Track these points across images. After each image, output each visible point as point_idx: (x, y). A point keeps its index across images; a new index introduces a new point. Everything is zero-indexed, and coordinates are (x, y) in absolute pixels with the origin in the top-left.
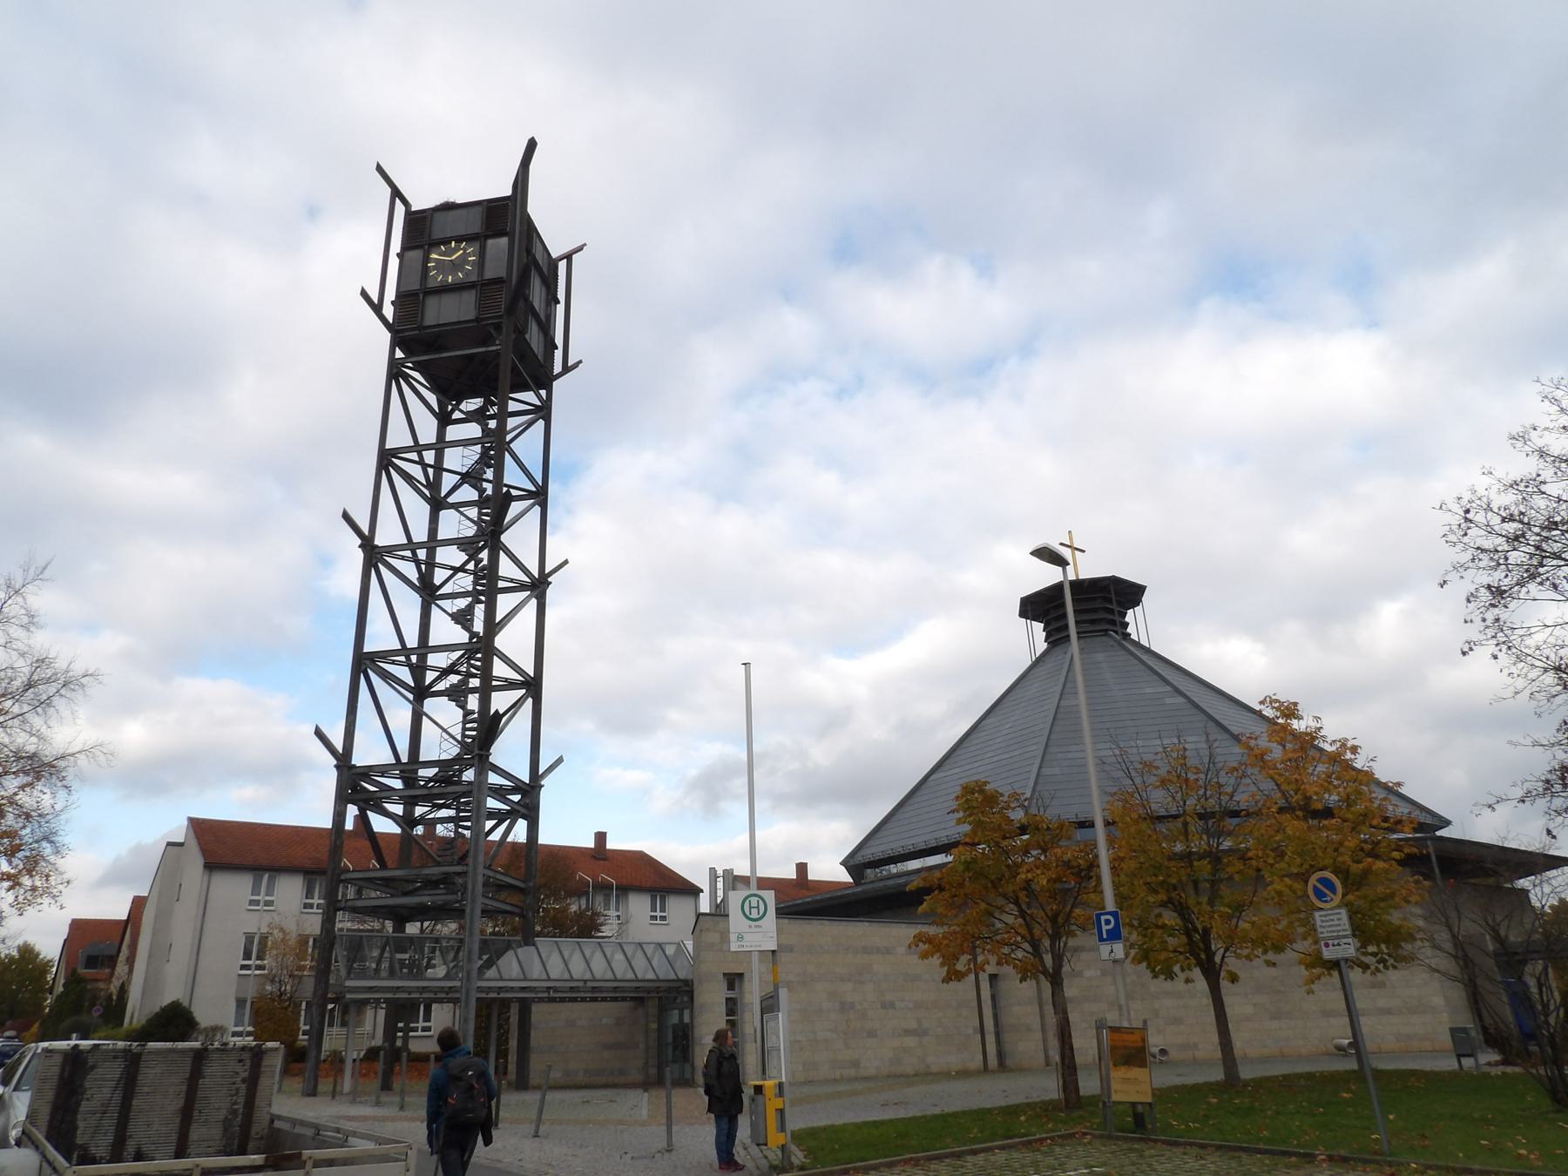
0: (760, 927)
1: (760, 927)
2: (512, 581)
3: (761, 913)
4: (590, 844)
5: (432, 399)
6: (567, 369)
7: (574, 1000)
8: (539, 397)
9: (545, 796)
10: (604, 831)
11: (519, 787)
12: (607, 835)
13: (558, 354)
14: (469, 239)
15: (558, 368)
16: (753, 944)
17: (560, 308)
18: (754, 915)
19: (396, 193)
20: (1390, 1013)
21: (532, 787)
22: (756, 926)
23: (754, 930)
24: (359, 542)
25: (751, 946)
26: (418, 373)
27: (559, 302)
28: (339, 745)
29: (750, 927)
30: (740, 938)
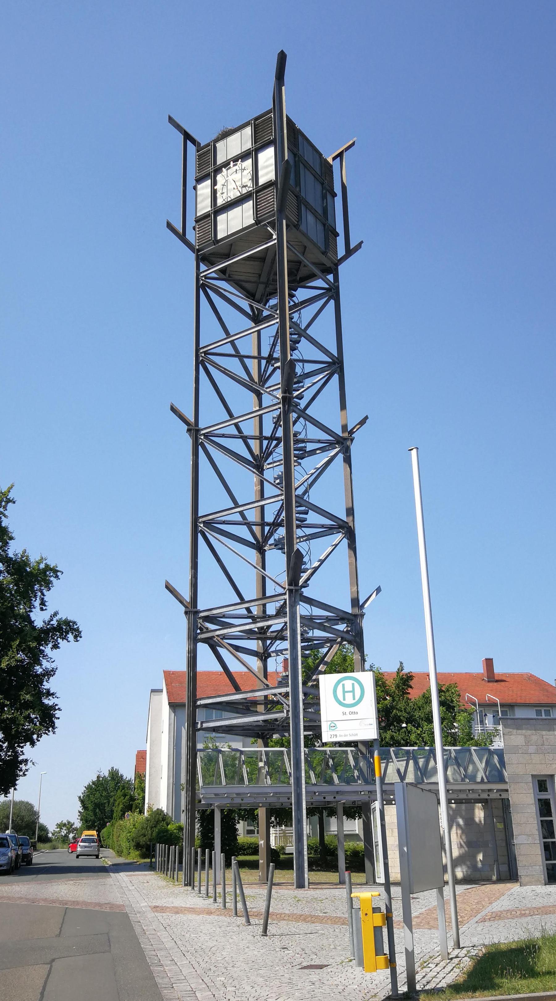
0: (357, 713)
1: (357, 713)
2: (319, 441)
3: (357, 696)
4: (479, 669)
5: (245, 304)
6: (349, 252)
7: (503, 804)
8: (327, 281)
9: (367, 625)
10: (491, 657)
11: (342, 617)
12: (493, 660)
13: (341, 241)
14: (243, 156)
15: (341, 252)
16: (347, 733)
17: (338, 201)
18: (349, 699)
19: (187, 137)
20: (488, 790)
21: (356, 616)
22: (352, 713)
23: (349, 717)
24: (186, 427)
25: (345, 736)
26: (224, 282)
27: (336, 195)
28: (187, 596)
29: (344, 714)
30: (333, 727)
